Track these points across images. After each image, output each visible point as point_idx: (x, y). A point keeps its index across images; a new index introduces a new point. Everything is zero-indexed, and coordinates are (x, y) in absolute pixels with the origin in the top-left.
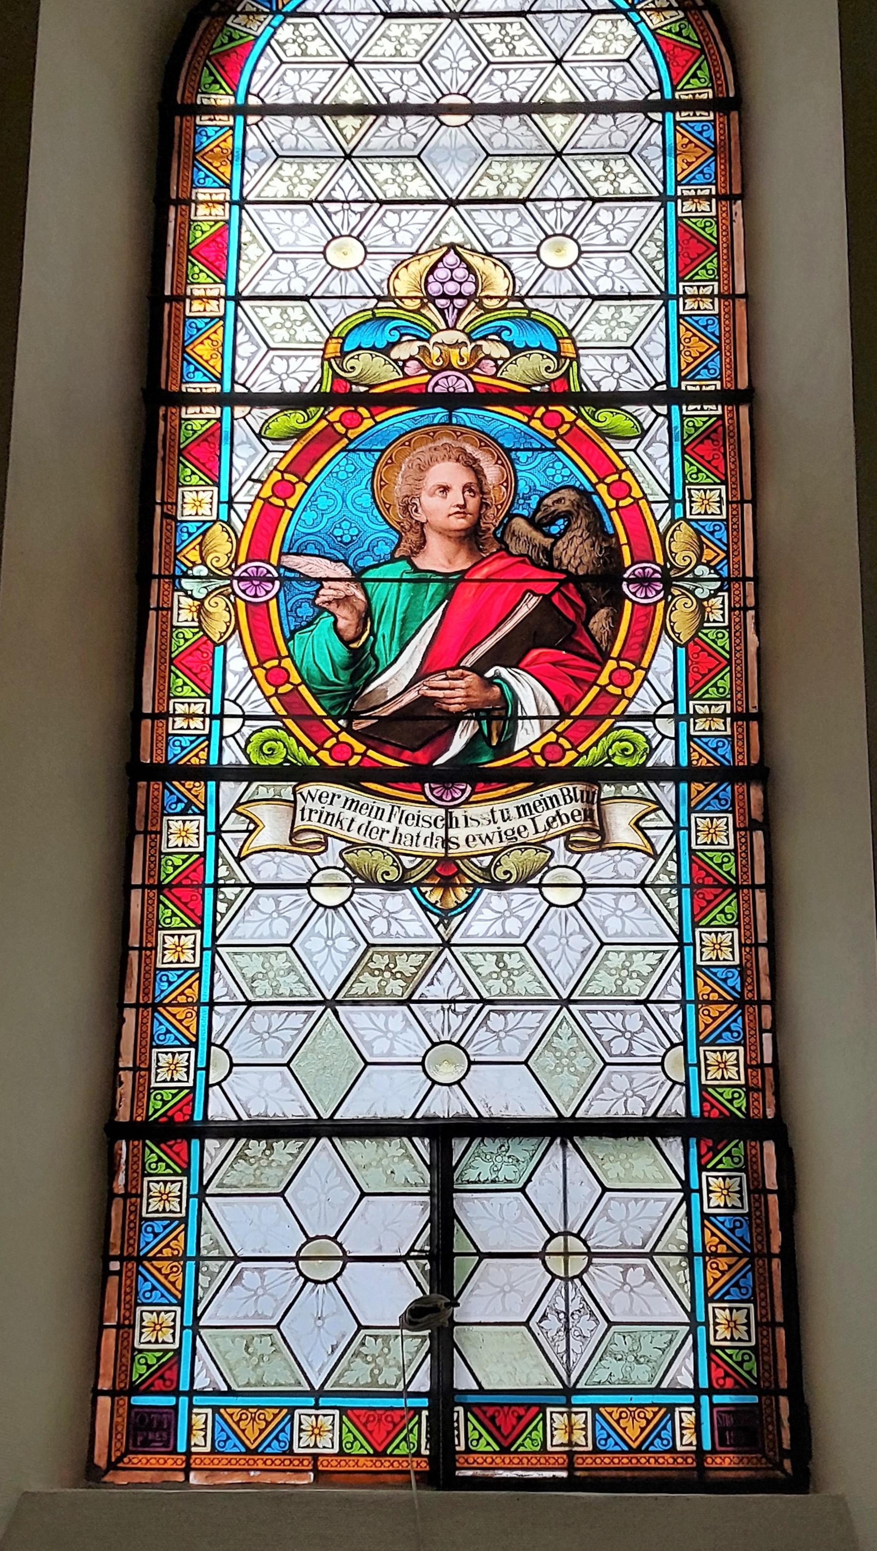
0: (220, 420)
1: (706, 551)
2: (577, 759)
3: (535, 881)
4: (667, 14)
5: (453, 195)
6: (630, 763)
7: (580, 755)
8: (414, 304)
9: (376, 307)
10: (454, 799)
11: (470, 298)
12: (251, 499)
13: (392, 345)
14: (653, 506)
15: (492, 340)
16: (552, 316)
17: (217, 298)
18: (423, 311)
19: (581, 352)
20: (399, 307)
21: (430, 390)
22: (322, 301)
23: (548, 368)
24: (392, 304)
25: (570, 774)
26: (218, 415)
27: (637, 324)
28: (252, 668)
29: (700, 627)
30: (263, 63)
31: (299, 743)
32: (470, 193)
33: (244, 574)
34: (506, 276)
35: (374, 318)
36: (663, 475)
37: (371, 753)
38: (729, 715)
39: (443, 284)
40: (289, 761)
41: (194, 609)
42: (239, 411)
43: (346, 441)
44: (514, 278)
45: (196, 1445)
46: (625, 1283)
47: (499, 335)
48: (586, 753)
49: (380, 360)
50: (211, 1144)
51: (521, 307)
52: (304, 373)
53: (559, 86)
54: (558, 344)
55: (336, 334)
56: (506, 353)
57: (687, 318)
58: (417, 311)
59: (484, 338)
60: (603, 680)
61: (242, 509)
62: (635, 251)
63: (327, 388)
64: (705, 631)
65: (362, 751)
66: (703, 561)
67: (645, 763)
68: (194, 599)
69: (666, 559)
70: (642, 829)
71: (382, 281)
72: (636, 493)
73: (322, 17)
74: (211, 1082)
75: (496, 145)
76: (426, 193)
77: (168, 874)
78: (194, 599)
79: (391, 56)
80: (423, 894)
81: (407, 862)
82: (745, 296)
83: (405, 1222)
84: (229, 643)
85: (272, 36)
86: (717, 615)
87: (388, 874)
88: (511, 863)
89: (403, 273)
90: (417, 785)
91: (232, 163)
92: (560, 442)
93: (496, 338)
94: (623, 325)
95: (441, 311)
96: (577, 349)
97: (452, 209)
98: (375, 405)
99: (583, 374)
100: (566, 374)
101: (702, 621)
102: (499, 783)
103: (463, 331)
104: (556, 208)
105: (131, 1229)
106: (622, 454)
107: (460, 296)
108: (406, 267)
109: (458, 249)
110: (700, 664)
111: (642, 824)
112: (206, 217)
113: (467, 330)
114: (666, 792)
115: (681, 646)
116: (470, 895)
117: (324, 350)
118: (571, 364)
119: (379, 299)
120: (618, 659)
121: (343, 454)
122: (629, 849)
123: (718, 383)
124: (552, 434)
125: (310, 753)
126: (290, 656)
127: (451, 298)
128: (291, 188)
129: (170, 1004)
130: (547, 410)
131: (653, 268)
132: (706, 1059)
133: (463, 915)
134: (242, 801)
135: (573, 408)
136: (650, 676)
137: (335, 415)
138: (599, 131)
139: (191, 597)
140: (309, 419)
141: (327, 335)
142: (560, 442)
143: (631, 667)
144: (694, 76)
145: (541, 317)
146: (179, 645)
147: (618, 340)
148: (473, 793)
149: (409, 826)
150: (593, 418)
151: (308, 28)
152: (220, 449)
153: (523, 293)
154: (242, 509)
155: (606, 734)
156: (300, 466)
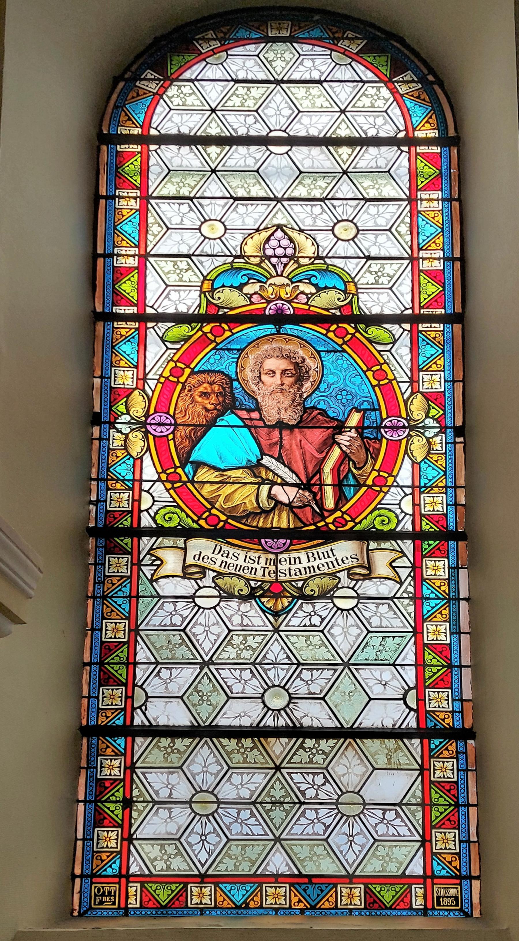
2: (354, 527)
5: (280, 196)
6: (386, 528)
7: (356, 524)
8: (257, 260)
9: (233, 261)
11: (291, 258)
12: (158, 377)
14: (400, 384)
16: (342, 269)
19: (359, 291)
20: (247, 263)
21: (267, 313)
22: (200, 258)
23: (339, 299)
24: (243, 261)
25: (351, 535)
28: (159, 474)
35: (232, 268)
39: (274, 249)
43: (214, 344)
44: (318, 246)
47: (309, 279)
48: (360, 522)
49: (236, 293)
50: (139, 740)
52: (188, 301)
55: (208, 278)
56: (313, 290)
58: (259, 265)
59: (300, 281)
62: (393, 230)
63: (203, 311)
68: (122, 434)
69: (407, 415)
70: (394, 568)
72: (390, 376)
75: (305, 166)
78: (122, 434)
80: (263, 603)
84: (144, 457)
86: (438, 447)
87: (242, 590)
92: (345, 346)
95: (274, 266)
96: (357, 289)
98: (231, 322)
99: (361, 304)
100: (351, 302)
101: (430, 449)
103: (287, 277)
107: (285, 256)
111: (394, 564)
113: (290, 277)
114: (408, 546)
117: (201, 287)
119: (236, 257)
122: (385, 578)
124: (340, 341)
127: (279, 257)
129: (106, 801)
130: (338, 327)
135: (353, 325)
137: (207, 328)
138: (371, 158)
139: (121, 432)
141: (202, 278)
142: (345, 346)
153: (324, 255)
155: (371, 512)
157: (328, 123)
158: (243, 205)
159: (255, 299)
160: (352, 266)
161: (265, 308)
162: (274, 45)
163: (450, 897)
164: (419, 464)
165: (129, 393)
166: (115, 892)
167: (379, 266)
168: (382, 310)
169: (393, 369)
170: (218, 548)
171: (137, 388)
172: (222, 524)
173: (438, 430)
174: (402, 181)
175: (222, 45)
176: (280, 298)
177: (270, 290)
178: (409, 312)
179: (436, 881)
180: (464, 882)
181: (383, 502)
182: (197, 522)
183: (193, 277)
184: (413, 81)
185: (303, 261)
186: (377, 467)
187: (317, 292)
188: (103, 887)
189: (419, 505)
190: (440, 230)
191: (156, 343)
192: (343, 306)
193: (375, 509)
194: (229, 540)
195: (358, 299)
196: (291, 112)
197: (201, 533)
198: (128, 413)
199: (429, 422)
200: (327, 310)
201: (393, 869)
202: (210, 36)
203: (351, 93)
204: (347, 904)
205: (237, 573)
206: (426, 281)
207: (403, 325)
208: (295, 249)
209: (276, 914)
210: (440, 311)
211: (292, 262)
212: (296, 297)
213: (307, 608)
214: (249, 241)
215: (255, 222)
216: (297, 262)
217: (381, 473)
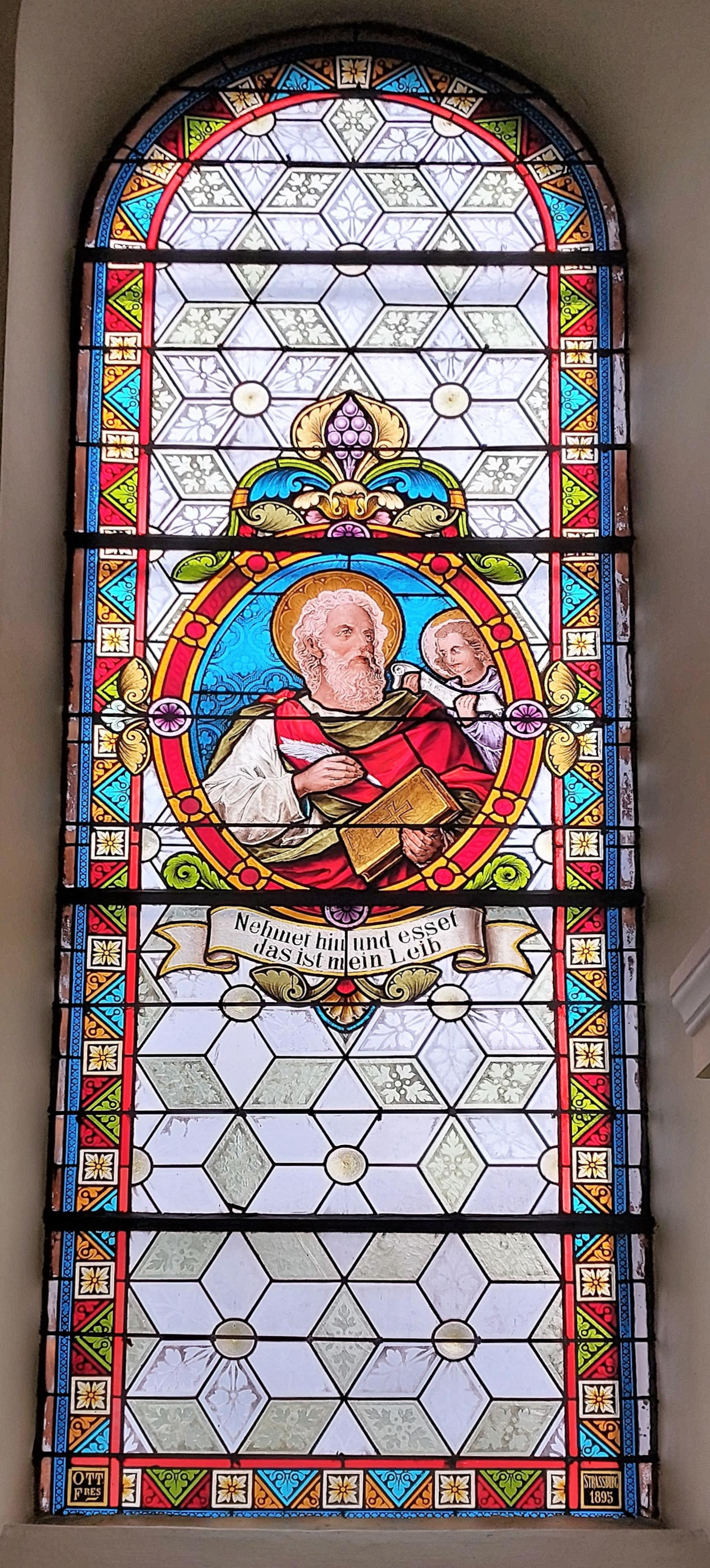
1: (581, 690)
2: (466, 883)
3: (424, 999)
4: (554, 168)
6: (514, 887)
7: (469, 879)
8: (316, 454)
9: (279, 457)
11: (367, 449)
12: (166, 638)
13: (294, 496)
14: (533, 648)
15: (387, 492)
19: (469, 503)
20: (302, 459)
23: (438, 518)
25: (462, 898)
28: (167, 799)
31: (212, 868)
32: (369, 157)
33: (157, 713)
36: (547, 1027)
37: (275, 877)
38: (596, 446)
39: (342, 433)
40: (203, 885)
41: (113, 741)
42: (154, 554)
45: (126, 1501)
48: (473, 877)
49: (283, 511)
52: (211, 521)
53: (449, 237)
56: (400, 505)
57: (568, 372)
59: (379, 490)
60: (488, 808)
64: (581, 764)
66: (579, 698)
67: (527, 886)
68: (113, 732)
69: (545, 696)
72: (517, 635)
73: (227, 165)
74: (133, 1182)
78: (113, 732)
81: (312, 981)
84: (145, 773)
85: (180, 184)
88: (403, 980)
89: (306, 421)
90: (317, 908)
94: (509, 476)
95: (340, 462)
96: (466, 500)
97: (351, 357)
100: (456, 523)
102: (393, 906)
103: (360, 483)
108: (308, 414)
111: (522, 947)
113: (364, 482)
114: (544, 914)
115: (559, 777)
117: (231, 500)
118: (460, 514)
120: (501, 790)
122: (509, 969)
125: (220, 877)
127: (349, 449)
128: (198, 333)
129: (87, 1334)
133: (359, 1030)
134: (161, 923)
136: (530, 805)
137: (242, 558)
139: (109, 729)
141: (234, 485)
143: (513, 797)
145: (431, 468)
147: (504, 205)
149: (312, 944)
150: (479, 564)
151: (214, 176)
155: (490, 860)
156: (210, 607)
159: (312, 517)
160: (457, 464)
161: (327, 530)
163: (606, 1490)
164: (562, 777)
165: (122, 664)
166: (102, 1481)
169: (522, 624)
171: (135, 656)
172: (263, 882)
176: (348, 517)
178: (546, 534)
179: (585, 1464)
181: (508, 843)
182: (225, 879)
183: (220, 485)
184: (557, 161)
185: (384, 455)
187: (406, 507)
188: (84, 1473)
189: (563, 846)
191: (163, 584)
192: (445, 527)
194: (281, 909)
197: (233, 898)
199: (579, 710)
206: (571, 483)
207: (538, 555)
208: (373, 433)
209: (343, 1515)
210: (592, 533)
211: (369, 455)
212: (374, 516)
215: (315, 386)
216: (377, 456)
217: (506, 794)
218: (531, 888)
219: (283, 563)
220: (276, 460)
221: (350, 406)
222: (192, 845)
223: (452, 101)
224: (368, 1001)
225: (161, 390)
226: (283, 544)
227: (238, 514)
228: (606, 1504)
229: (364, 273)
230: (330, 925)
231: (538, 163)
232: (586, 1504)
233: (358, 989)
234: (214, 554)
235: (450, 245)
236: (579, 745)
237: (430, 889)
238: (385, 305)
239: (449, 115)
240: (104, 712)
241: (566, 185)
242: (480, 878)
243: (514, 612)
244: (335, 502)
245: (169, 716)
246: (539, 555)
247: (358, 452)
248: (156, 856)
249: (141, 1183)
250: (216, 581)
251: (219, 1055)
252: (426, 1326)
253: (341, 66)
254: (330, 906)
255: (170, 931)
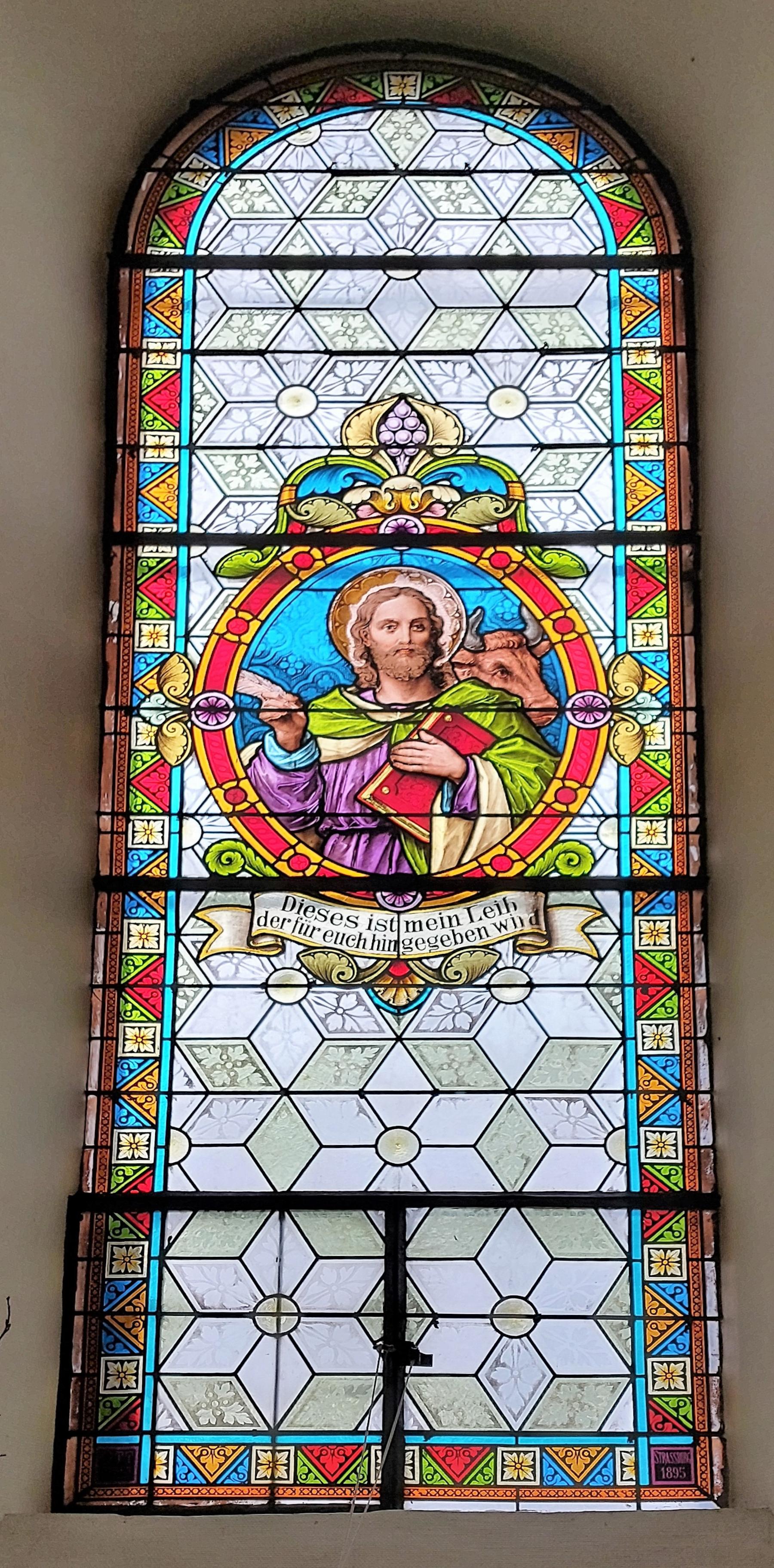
0: (176, 559)
3: (483, 981)
6: (576, 873)
7: (529, 866)
8: (367, 452)
9: (329, 455)
10: (406, 904)
11: (420, 446)
13: (344, 491)
17: (174, 352)
18: (374, 458)
20: (352, 456)
23: (497, 509)
24: (345, 452)
25: (521, 883)
26: (174, 555)
27: (585, 469)
29: (643, 750)
30: (211, 219)
34: (456, 425)
39: (394, 432)
41: (152, 734)
42: (196, 550)
44: (464, 428)
46: (556, 421)
48: (533, 864)
51: (471, 460)
52: (260, 518)
53: (503, 241)
54: (508, 488)
56: (456, 497)
58: (369, 458)
59: (434, 483)
61: (199, 643)
63: (281, 529)
65: (318, 861)
66: (646, 688)
68: (152, 725)
69: (609, 688)
70: (588, 935)
71: (335, 430)
72: (581, 628)
74: (171, 1161)
76: (375, 345)
77: (130, 973)
78: (152, 725)
79: (339, 212)
81: (362, 963)
82: (720, 1433)
83: (363, 1280)
84: (186, 764)
87: (343, 973)
91: (182, 313)
92: (507, 582)
93: (447, 483)
95: (394, 459)
96: (525, 492)
99: (530, 516)
100: (513, 516)
102: (444, 891)
103: (414, 477)
104: (504, 361)
105: (125, 661)
106: (567, 592)
109: (410, 400)
110: (642, 783)
111: (587, 930)
112: (157, 367)
114: (609, 898)
116: (421, 994)
117: (279, 496)
118: (518, 507)
121: (296, 593)
123: (658, 340)
125: (266, 862)
126: (247, 777)
127: (403, 447)
131: (610, 1003)
132: (650, 1256)
135: (520, 548)
139: (149, 722)
140: (263, 559)
144: (638, 234)
146: (138, 766)
148: (424, 899)
149: (362, 928)
152: (176, 583)
154: (199, 643)
155: (551, 847)
156: (254, 604)
157: (480, 238)
158: (345, 362)
160: (518, 460)
162: (395, 114)
167: (561, 457)
168: (565, 526)
169: (585, 617)
170: (291, 900)
173: (659, 712)
174: (597, 322)
175: (311, 116)
176: (401, 511)
177: (387, 497)
180: (627, 441)
182: (272, 866)
183: (266, 482)
184: (614, 171)
185: (439, 452)
186: (560, 773)
190: (665, 683)
193: (556, 842)
194: (329, 894)
195: (526, 508)
196: (421, 219)
197: (282, 883)
198: (161, 691)
200: (477, 526)
201: (588, 1422)
202: (289, 100)
203: (517, 189)
204: (512, 1479)
205: (338, 946)
211: (424, 452)
212: (429, 509)
213: (449, 999)
214: (355, 421)
218: (593, 874)
219: (330, 560)
220: (326, 457)
221: (402, 409)
222: (236, 832)
223: (507, 112)
224: (423, 983)
225: (202, 394)
226: (331, 540)
227: (285, 510)
228: (679, 1479)
229: (415, 277)
230: (382, 908)
231: (595, 171)
232: (657, 1480)
233: (412, 971)
234: (260, 550)
235: (503, 250)
236: (645, 735)
237: (488, 876)
238: (437, 308)
239: (502, 125)
240: (143, 706)
241: (625, 192)
242: (541, 863)
243: (577, 605)
244: (387, 497)
245: (213, 710)
246: (601, 548)
247: (412, 450)
248: (198, 843)
249: (178, 1163)
250: (256, 582)
251: (258, 1039)
252: (486, 1303)
253: (389, 81)
254: (381, 891)
255: (214, 916)
